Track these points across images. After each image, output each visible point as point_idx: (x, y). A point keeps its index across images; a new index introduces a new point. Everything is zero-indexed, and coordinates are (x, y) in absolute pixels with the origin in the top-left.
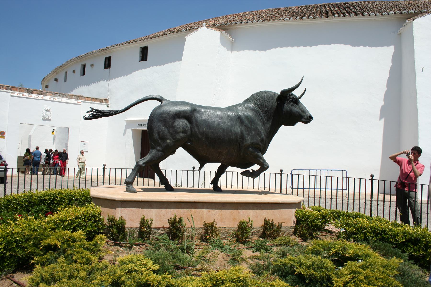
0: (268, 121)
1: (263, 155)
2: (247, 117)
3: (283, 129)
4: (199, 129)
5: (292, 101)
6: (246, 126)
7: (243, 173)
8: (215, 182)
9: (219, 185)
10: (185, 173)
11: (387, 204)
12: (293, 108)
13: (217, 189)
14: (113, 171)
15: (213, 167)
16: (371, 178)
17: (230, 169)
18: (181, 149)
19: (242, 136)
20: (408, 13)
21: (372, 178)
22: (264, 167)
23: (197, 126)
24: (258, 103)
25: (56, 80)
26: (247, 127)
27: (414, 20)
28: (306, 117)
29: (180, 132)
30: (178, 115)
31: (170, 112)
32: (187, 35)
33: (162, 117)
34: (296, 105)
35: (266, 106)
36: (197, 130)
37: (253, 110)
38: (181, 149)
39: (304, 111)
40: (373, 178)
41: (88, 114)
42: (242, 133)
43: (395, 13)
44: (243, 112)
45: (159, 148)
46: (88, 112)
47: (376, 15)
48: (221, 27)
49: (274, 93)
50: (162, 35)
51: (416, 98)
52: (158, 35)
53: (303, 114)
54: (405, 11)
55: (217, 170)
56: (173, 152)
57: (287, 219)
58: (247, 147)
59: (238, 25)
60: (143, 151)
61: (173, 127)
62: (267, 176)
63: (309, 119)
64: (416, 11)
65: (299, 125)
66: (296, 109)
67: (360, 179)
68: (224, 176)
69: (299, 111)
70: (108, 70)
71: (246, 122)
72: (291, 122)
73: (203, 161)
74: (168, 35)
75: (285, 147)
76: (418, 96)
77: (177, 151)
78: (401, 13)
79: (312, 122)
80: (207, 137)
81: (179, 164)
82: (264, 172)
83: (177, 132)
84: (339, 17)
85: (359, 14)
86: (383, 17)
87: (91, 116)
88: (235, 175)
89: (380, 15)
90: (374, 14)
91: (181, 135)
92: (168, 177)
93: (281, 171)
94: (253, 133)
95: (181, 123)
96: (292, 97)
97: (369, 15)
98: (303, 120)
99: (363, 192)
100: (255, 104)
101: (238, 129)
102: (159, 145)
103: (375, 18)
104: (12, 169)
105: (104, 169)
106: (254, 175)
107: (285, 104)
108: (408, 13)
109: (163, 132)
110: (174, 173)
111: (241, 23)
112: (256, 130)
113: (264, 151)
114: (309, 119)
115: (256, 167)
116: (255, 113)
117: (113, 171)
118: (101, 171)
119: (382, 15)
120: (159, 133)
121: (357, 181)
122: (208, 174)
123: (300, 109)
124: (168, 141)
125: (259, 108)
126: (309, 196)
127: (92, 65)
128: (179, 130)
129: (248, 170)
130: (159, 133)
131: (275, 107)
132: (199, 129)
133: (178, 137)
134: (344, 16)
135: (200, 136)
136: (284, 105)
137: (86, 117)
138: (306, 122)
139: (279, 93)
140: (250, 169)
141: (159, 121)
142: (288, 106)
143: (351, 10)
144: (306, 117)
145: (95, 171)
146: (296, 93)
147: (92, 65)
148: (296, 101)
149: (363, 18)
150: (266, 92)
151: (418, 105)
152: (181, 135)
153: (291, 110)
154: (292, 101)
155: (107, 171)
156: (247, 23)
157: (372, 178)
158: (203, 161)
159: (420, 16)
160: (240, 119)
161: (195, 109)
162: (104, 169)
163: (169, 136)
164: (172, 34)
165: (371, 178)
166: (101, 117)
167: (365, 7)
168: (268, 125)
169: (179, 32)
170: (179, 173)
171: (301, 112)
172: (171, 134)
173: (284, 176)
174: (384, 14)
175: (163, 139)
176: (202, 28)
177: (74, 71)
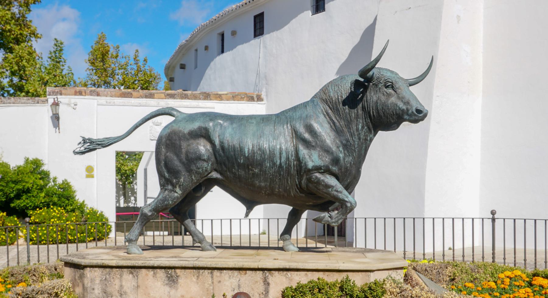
3: (381, 134)
16: (491, 216)
25: (183, 67)
26: (305, 142)
40: (496, 216)
73: (250, 204)
93: (493, 213)
99: (478, 243)
121: (448, 222)
147: (234, 33)
158: (250, 204)
177: (206, 48)
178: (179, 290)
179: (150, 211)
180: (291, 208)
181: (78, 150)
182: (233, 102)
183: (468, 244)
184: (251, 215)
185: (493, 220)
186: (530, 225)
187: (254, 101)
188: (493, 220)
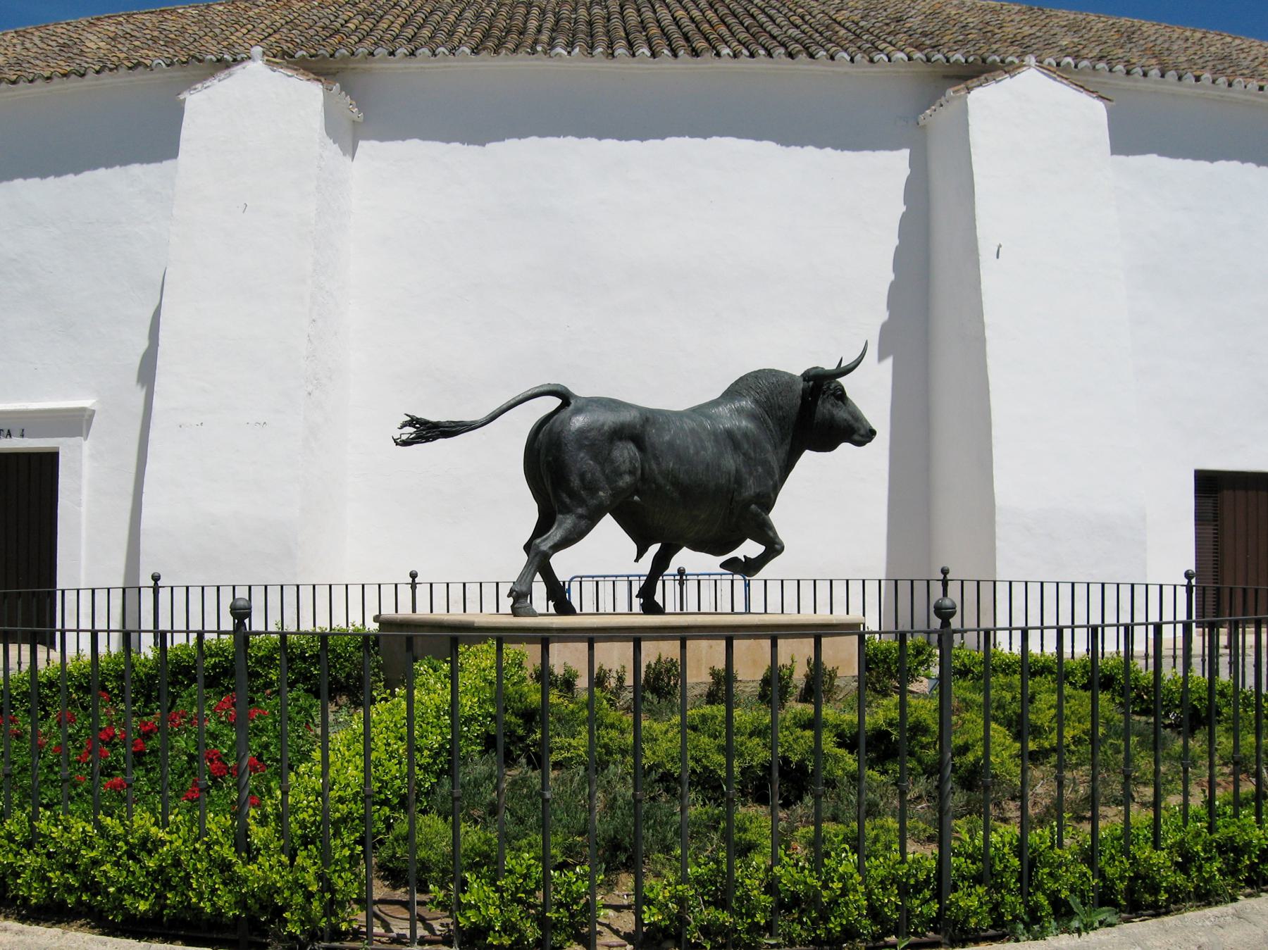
0: (783, 440)
2: (745, 435)
3: (808, 457)
4: (659, 464)
5: (833, 394)
6: (744, 454)
9: (658, 598)
12: (835, 411)
16: (941, 577)
19: (739, 480)
20: (948, 61)
22: (773, 548)
23: (656, 458)
27: (969, 90)
28: (862, 432)
29: (625, 472)
30: (621, 433)
31: (603, 425)
32: (189, 85)
33: (586, 438)
35: (780, 408)
36: (654, 466)
37: (752, 416)
39: (857, 417)
43: (910, 59)
44: (728, 419)
45: (580, 511)
47: (852, 60)
48: (316, 67)
50: (64, 75)
51: (982, 341)
52: (47, 74)
53: (856, 425)
54: (940, 56)
57: (842, 657)
58: (747, 504)
59: (380, 60)
61: (612, 462)
64: (971, 59)
65: (845, 447)
66: (841, 414)
69: (850, 418)
71: (746, 446)
72: (826, 442)
74: (91, 75)
76: (988, 333)
78: (929, 60)
80: (676, 483)
83: (618, 473)
84: (735, 56)
85: (799, 52)
86: (873, 69)
89: (865, 61)
90: (845, 55)
91: (627, 478)
94: (760, 469)
95: (625, 453)
97: (832, 58)
98: (856, 437)
100: (756, 401)
101: (730, 462)
102: (582, 502)
103: (849, 68)
107: (820, 402)
108: (948, 61)
109: (593, 474)
111: (392, 54)
112: (765, 463)
115: (750, 549)
119: (871, 61)
120: (582, 476)
123: (850, 413)
124: (601, 493)
128: (623, 468)
130: (582, 476)
131: (797, 409)
132: (659, 464)
133: (621, 483)
134: (752, 55)
135: (661, 480)
136: (816, 405)
138: (860, 444)
141: (581, 447)
142: (825, 407)
143: (761, 26)
144: (862, 432)
149: (812, 67)
151: (989, 361)
152: (627, 478)
153: (832, 416)
154: (833, 394)
156: (412, 54)
159: (987, 81)
160: (731, 439)
161: (650, 418)
163: (603, 483)
164: (106, 73)
165: (941, 577)
167: (802, 17)
168: (783, 452)
169: (141, 68)
171: (852, 422)
172: (607, 478)
174: (876, 59)
175: (592, 488)
176: (250, 65)
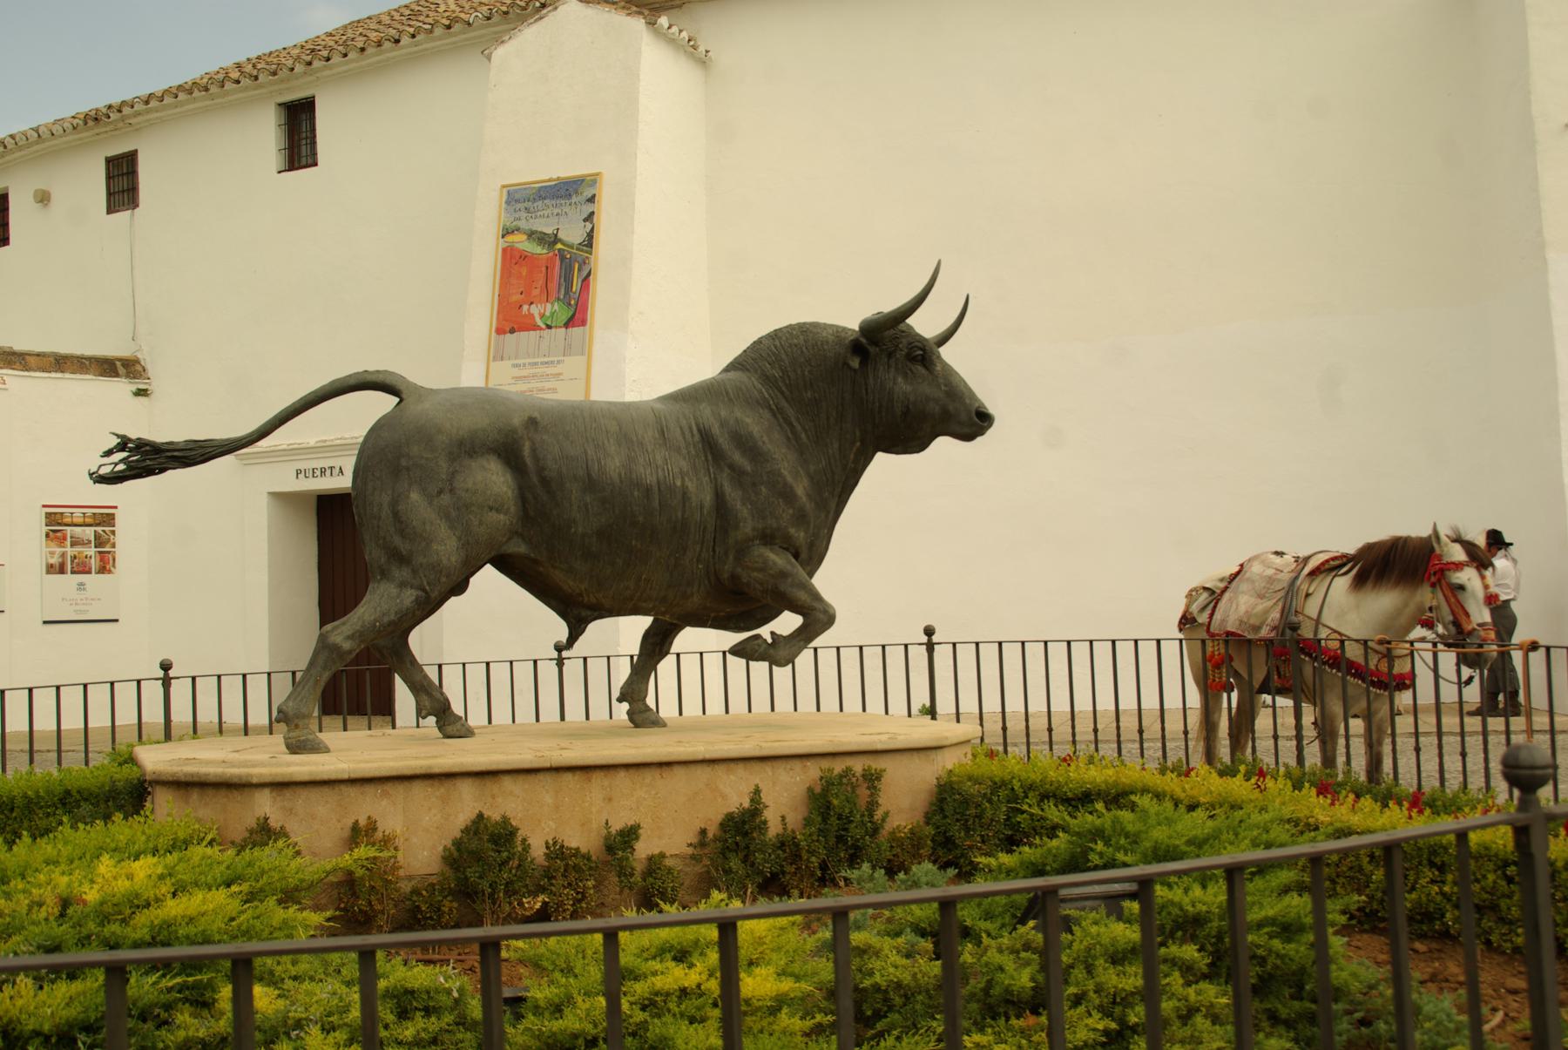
1: (811, 575)
3: (883, 465)
7: (737, 651)
8: (633, 693)
10: (524, 673)
11: (1451, 742)
13: (643, 717)
14: (207, 688)
15: (624, 634)
16: (925, 639)
17: (690, 639)
18: (488, 566)
21: (930, 640)
22: (817, 619)
24: (777, 373)
26: (738, 474)
30: (468, 448)
34: (920, 369)
38: (489, 569)
40: (935, 639)
41: (106, 460)
42: (720, 503)
46: (109, 453)
49: (839, 331)
55: (636, 651)
56: (460, 587)
60: (335, 597)
62: (827, 659)
63: (972, 422)
67: (1158, 641)
68: (666, 666)
70: (123, 217)
73: (578, 614)
75: (895, 536)
77: (474, 581)
79: (990, 432)
81: (487, 631)
82: (814, 644)
87: (121, 467)
88: (713, 664)
92: (453, 690)
93: (166, 666)
96: (904, 341)
104: (139, 682)
105: (166, 682)
106: (779, 653)
110: (476, 675)
113: (813, 555)
114: (972, 422)
115: (787, 623)
116: (767, 414)
117: (207, 688)
118: (153, 692)
121: (1102, 651)
122: (597, 668)
125: (782, 393)
126: (1163, 737)
127: (43, 198)
129: (758, 637)
137: (102, 472)
138: (968, 437)
139: (857, 328)
140: (765, 632)
145: (126, 694)
146: (925, 324)
147: (43, 198)
148: (923, 355)
150: (804, 330)
155: (180, 691)
157: (930, 640)
158: (578, 614)
162: (166, 682)
166: (162, 470)
170: (500, 674)
173: (942, 655)
178: (1387, 812)
179: (348, 638)
180: (646, 621)
181: (105, 470)
182: (59, 375)
183: (1037, 705)
184: (583, 645)
185: (930, 647)
186: (1058, 653)
187: (117, 375)
188: (930, 647)
